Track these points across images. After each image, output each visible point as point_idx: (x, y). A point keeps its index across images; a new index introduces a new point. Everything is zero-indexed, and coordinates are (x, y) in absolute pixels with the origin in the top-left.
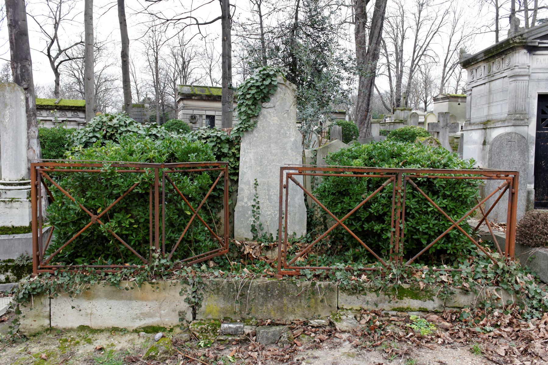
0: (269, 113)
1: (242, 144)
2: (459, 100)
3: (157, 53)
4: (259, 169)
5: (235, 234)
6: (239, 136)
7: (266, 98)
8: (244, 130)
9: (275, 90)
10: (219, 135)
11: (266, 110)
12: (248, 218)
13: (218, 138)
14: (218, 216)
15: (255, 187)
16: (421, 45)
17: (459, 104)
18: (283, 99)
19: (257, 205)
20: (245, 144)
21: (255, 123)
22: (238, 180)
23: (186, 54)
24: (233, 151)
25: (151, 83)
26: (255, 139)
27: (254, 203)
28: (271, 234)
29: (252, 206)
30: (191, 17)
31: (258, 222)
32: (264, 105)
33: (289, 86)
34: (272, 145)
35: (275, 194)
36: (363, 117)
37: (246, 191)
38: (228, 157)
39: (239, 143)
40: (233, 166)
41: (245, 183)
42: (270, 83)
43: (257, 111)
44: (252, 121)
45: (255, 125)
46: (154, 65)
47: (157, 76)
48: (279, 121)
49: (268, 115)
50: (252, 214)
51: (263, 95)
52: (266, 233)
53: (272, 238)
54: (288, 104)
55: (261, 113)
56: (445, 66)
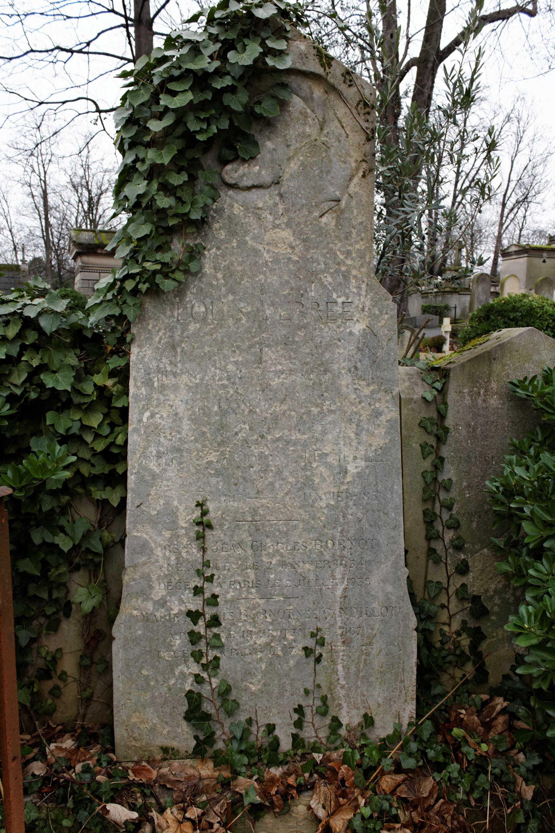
0: (256, 212)
1: (134, 350)
2: (545, 255)
3: (45, 182)
4: (212, 457)
5: (119, 732)
6: (122, 318)
7: (237, 143)
8: (143, 287)
9: (283, 104)
10: (31, 313)
11: (241, 196)
12: (172, 667)
13: (29, 324)
14: (51, 644)
15: (200, 537)
16: (468, 171)
17: (544, 261)
18: (314, 146)
19: (209, 612)
20: (148, 352)
21: (194, 254)
22: (123, 500)
23: (94, 184)
24: (98, 379)
25: (39, 233)
26: (193, 327)
27: (195, 604)
28: (271, 728)
29: (189, 613)
30: (87, 99)
31: (215, 682)
32: (234, 172)
33: (343, 87)
34: (269, 354)
35: (283, 564)
36: (394, 283)
37: (159, 552)
38: (79, 406)
39: (122, 348)
40: (100, 446)
41: (154, 522)
42: (260, 60)
43: (201, 200)
44: (178, 248)
45: (193, 267)
46: (40, 201)
47: (47, 219)
48: (300, 248)
49: (251, 219)
50: (189, 648)
51: (225, 125)
52: (250, 721)
53: (275, 744)
54: (339, 170)
55: (220, 211)
56: (504, 205)
